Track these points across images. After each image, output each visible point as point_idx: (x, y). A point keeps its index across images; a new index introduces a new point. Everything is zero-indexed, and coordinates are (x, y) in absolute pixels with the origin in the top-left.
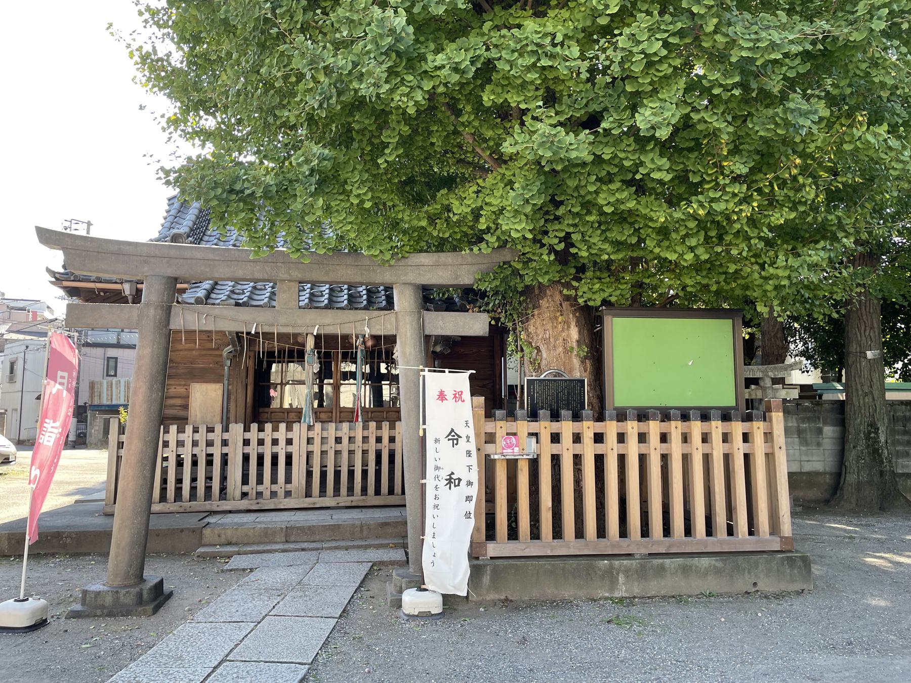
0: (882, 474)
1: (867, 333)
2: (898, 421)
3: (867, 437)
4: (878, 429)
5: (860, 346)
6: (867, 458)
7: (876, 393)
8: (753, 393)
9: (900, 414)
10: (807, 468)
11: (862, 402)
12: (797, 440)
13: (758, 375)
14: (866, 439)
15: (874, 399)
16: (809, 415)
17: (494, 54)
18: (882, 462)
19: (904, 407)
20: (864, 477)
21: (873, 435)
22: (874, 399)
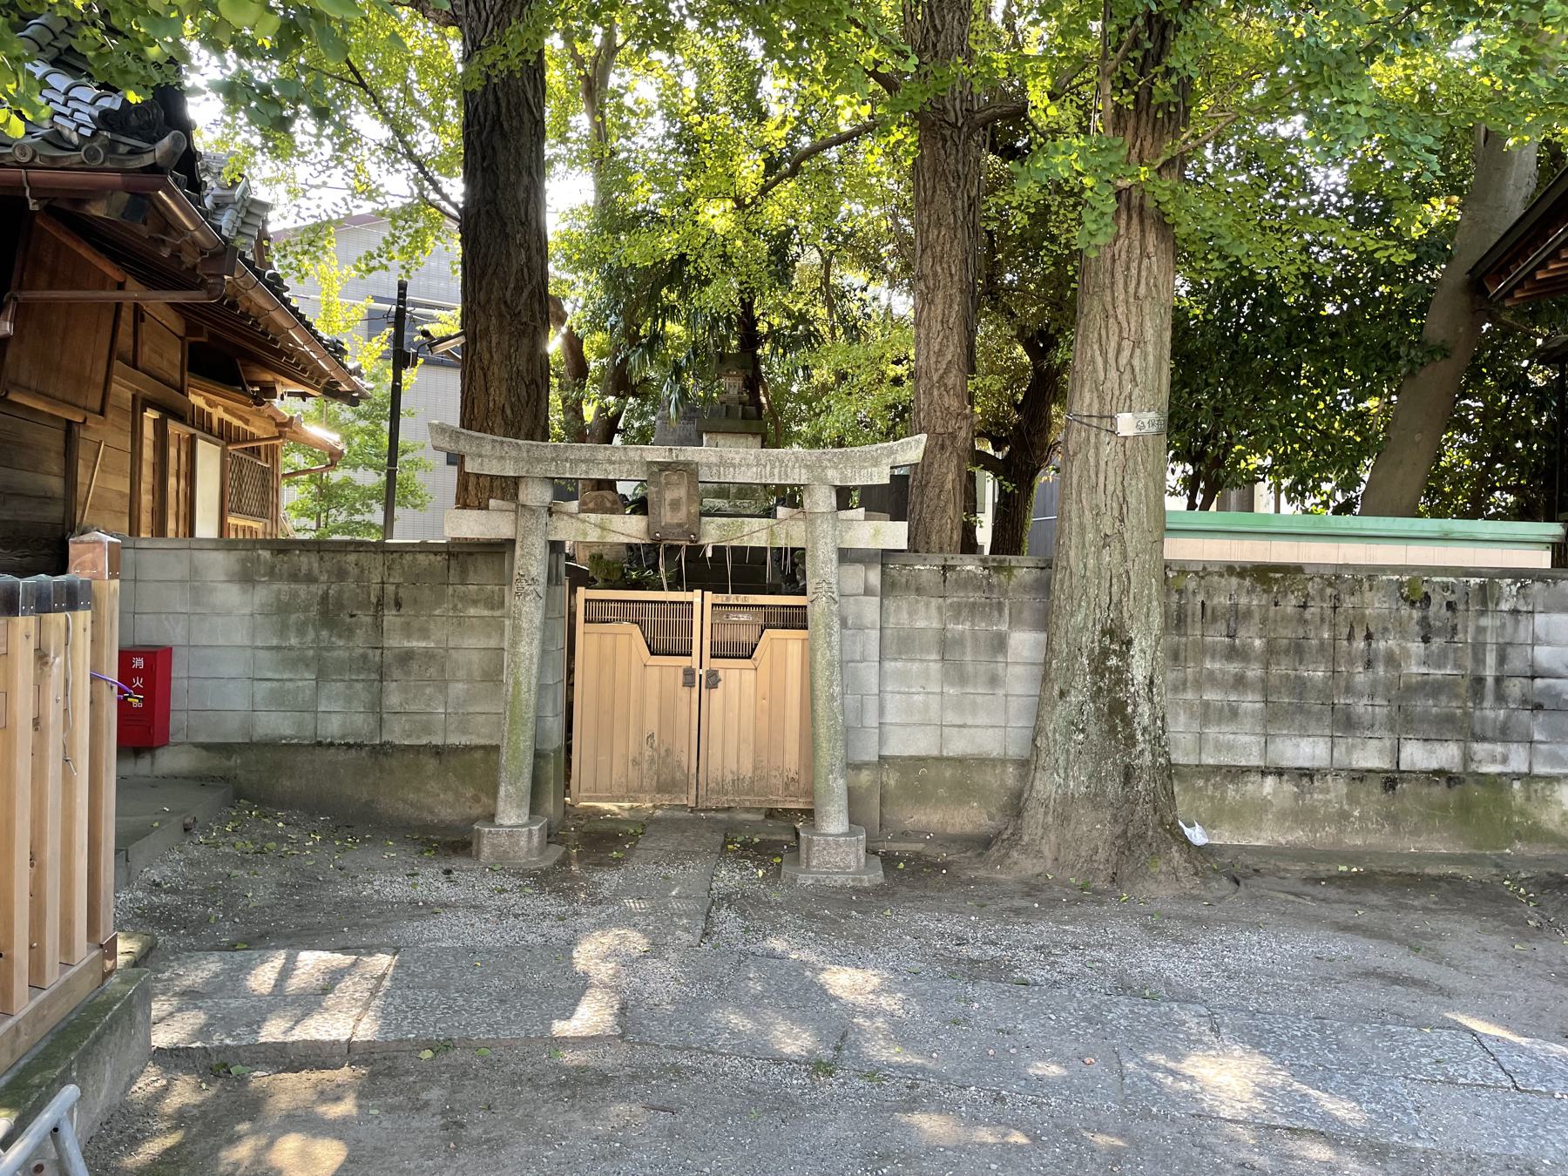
0: (1128, 775)
1: (1123, 361)
2: (1214, 619)
3: (1099, 668)
4: (1129, 642)
5: (1101, 398)
6: (1092, 729)
7: (1133, 540)
8: (781, 531)
9: (1221, 600)
10: (958, 746)
11: (1091, 562)
12: (935, 667)
13: (797, 476)
14: (1094, 672)
15: (1125, 558)
16: (975, 597)
17: (1349, 234)
18: (1131, 740)
19: (1234, 581)
20: (1079, 782)
21: (1113, 661)
22: (1125, 558)
